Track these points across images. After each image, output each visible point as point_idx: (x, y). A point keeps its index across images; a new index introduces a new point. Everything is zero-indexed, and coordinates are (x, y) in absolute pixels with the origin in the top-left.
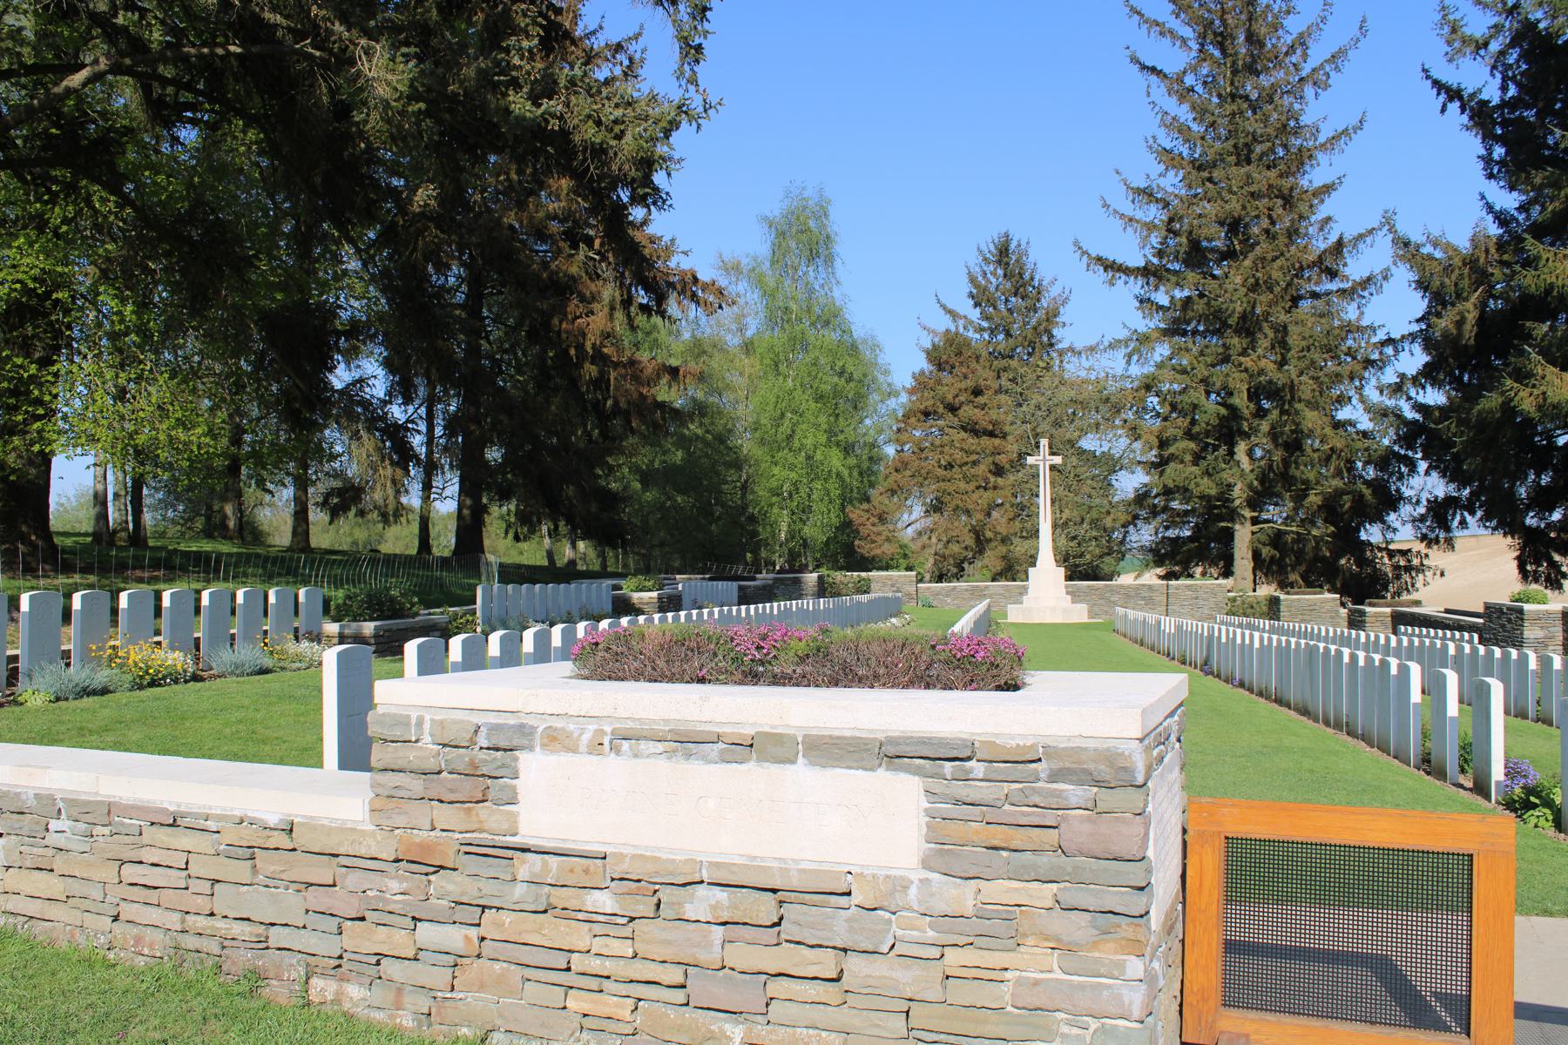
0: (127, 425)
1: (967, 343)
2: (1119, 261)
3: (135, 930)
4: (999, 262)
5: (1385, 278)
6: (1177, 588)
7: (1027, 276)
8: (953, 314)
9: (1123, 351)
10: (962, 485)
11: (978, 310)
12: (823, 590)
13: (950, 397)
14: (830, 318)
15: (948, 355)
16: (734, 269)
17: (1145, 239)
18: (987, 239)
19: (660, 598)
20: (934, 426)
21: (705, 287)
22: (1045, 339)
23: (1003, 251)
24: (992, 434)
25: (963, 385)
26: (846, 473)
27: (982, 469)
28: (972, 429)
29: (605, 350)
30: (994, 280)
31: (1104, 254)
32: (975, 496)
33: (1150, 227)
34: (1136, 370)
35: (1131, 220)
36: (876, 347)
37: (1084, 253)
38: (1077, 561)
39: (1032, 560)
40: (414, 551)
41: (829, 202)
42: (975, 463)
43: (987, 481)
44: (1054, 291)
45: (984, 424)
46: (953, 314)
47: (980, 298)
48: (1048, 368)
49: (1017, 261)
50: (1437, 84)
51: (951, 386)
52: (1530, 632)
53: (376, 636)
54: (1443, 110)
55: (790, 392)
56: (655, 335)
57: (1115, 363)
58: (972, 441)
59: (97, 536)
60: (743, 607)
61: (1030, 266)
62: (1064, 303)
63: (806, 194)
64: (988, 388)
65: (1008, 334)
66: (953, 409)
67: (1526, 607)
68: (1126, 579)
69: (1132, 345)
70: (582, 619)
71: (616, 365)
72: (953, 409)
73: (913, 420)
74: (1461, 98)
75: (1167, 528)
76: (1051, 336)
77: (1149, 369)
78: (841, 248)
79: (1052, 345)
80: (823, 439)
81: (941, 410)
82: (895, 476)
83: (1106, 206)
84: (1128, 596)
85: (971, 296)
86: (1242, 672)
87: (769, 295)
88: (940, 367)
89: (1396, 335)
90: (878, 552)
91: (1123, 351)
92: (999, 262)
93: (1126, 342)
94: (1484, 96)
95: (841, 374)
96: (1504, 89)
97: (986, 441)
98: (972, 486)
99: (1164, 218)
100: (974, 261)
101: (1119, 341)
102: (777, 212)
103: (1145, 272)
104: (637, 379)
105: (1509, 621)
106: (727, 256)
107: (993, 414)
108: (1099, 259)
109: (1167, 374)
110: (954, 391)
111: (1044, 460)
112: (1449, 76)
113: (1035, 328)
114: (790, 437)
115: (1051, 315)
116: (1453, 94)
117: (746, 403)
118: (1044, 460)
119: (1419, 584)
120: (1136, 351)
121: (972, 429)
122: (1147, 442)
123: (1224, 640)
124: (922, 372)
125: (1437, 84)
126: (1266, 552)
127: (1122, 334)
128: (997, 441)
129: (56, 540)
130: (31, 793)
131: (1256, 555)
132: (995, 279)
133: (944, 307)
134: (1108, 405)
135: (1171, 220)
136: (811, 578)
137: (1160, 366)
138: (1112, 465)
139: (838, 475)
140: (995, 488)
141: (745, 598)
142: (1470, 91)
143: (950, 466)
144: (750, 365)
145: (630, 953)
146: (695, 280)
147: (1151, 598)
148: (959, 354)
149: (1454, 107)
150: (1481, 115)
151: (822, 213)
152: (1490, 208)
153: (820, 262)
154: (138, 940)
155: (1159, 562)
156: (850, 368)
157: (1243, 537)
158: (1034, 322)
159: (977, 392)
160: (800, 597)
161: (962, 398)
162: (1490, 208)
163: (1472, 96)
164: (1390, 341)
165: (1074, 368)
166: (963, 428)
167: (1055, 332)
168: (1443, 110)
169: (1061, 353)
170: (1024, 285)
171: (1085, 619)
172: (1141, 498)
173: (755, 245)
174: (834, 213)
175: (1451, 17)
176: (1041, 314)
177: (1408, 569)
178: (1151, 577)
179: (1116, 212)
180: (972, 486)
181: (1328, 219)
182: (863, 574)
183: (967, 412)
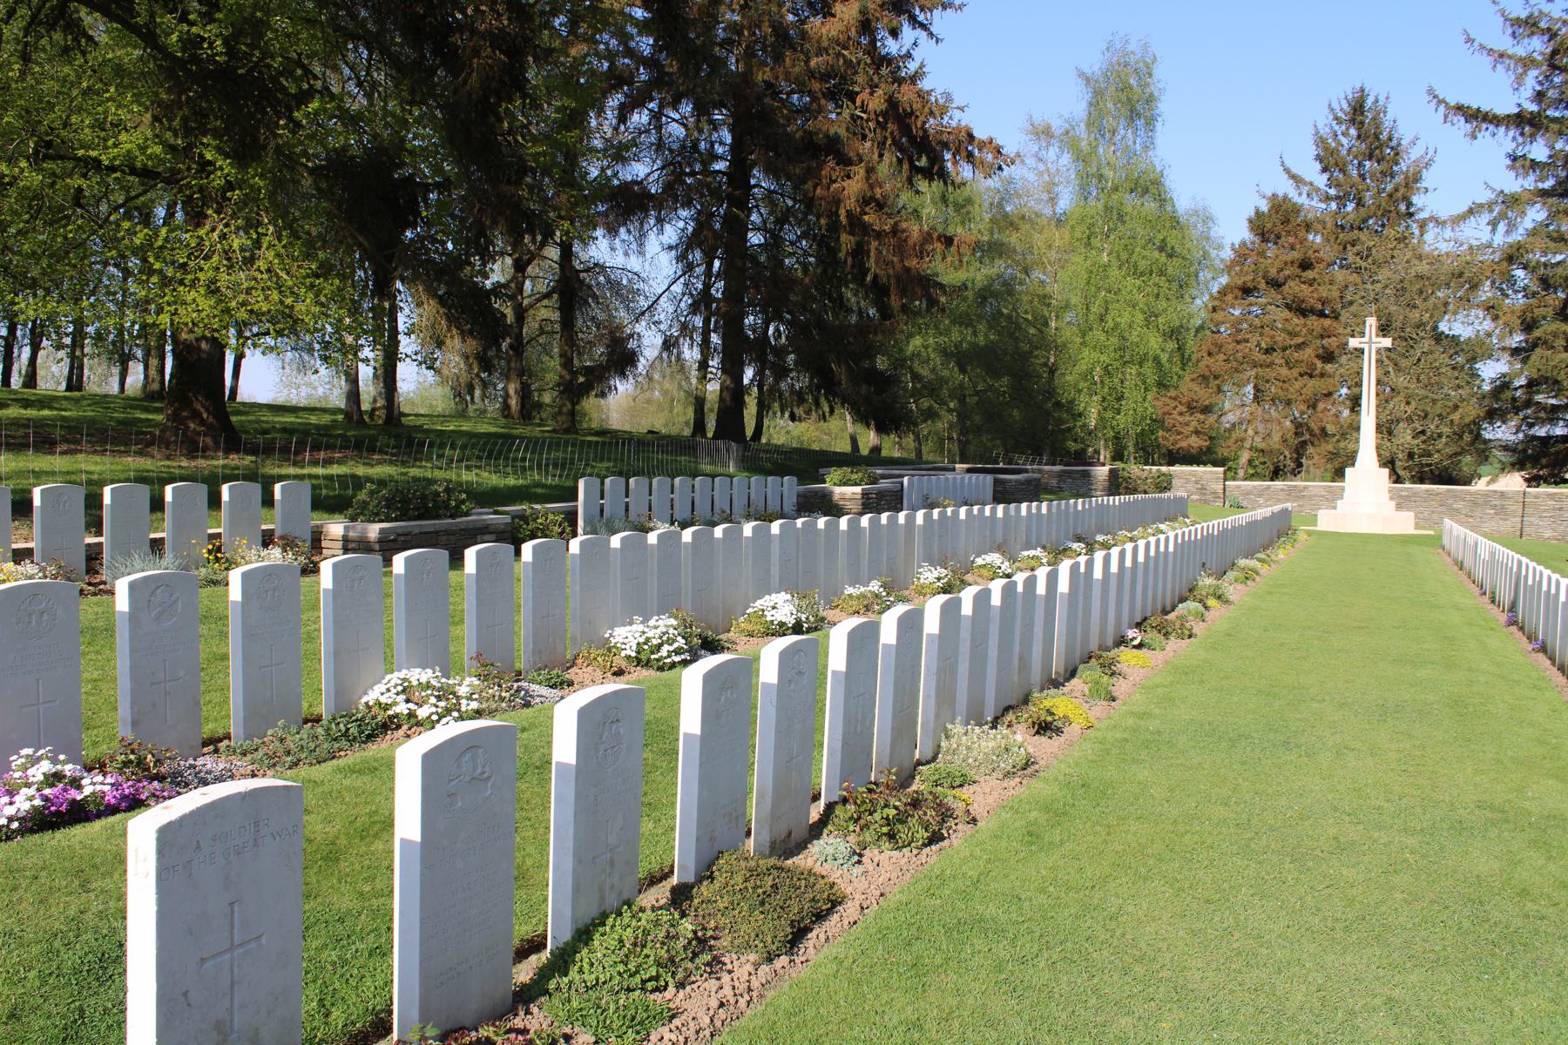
0: (132, 286)
1: (1296, 209)
2: (1485, 108)
4: (1353, 121)
6: (1536, 497)
7: (1384, 136)
8: (1295, 178)
9: (1486, 217)
10: (1284, 371)
11: (1326, 176)
12: (1116, 485)
14: (1150, 186)
15: (1276, 223)
16: (1043, 133)
17: (1520, 80)
18: (1339, 95)
19: (865, 494)
20: (1256, 305)
21: (982, 145)
22: (1403, 207)
23: (1357, 111)
24: (1321, 314)
25: (1289, 258)
26: (1164, 358)
27: (1308, 354)
28: (1300, 309)
29: (866, 218)
30: (1344, 141)
31: (1465, 102)
32: (1298, 385)
33: (1527, 63)
34: (1499, 239)
35: (1501, 56)
36: (1208, 219)
37: (1440, 102)
38: (1425, 460)
39: (1351, 459)
40: (687, 432)
41: (1155, 60)
42: (1299, 347)
43: (1313, 366)
44: (1415, 153)
45: (1312, 302)
46: (1295, 178)
47: (1329, 160)
48: (1402, 239)
49: (1374, 119)
51: (1275, 257)
53: (380, 541)
55: (1105, 267)
56: (969, 208)
57: (1477, 232)
58: (1297, 320)
59: (347, 414)
60: (1000, 508)
61: (1387, 124)
63: (1130, 48)
64: (1320, 261)
65: (1360, 204)
66: (1276, 284)
68: (1481, 485)
69: (1497, 209)
70: (748, 517)
71: (879, 235)
72: (1276, 284)
73: (1229, 297)
75: (1531, 426)
76: (1409, 204)
77: (1518, 236)
78: (1164, 107)
79: (1411, 215)
80: (1139, 318)
81: (1263, 285)
82: (1207, 361)
83: (1470, 40)
84: (1475, 504)
85: (1319, 158)
86: (1545, 634)
87: (1082, 158)
88: (1265, 240)
90: (1184, 444)
91: (1486, 217)
92: (1353, 121)
93: (1490, 206)
95: (1161, 249)
97: (1314, 322)
98: (1295, 372)
99: (1549, 51)
100: (1325, 122)
101: (1481, 206)
102: (1096, 68)
103: (1526, 123)
104: (901, 248)
106: (1037, 120)
107: (1324, 292)
108: (1459, 108)
109: (1540, 243)
110: (1278, 264)
111: (1370, 342)
113: (1390, 196)
114: (1102, 319)
115: (1412, 181)
117: (1060, 279)
118: (1370, 342)
120: (1502, 216)
121: (1300, 309)
122: (1506, 324)
123: (1530, 582)
124: (1243, 244)
127: (1484, 197)
128: (1327, 322)
129: (234, 419)
132: (1347, 140)
133: (1287, 171)
134: (1463, 279)
135: (1555, 52)
136: (1101, 472)
137: (1533, 233)
138: (1476, 351)
139: (1156, 360)
140: (1322, 375)
141: (1003, 495)
143: (1269, 351)
144: (1060, 237)
146: (971, 137)
148: (1286, 221)
151: (1145, 72)
153: (1140, 123)
155: (1519, 465)
156: (1171, 242)
158: (1389, 187)
159: (1305, 265)
160: (1087, 494)
161: (1287, 272)
165: (1437, 242)
166: (1288, 307)
167: (1415, 199)
169: (1423, 225)
170: (1380, 147)
171: (1410, 529)
172: (1503, 385)
173: (1067, 104)
174: (1158, 72)
176: (1399, 179)
178: (1513, 482)
179: (1482, 47)
180: (1295, 372)
182: (1164, 469)
183: (1294, 288)
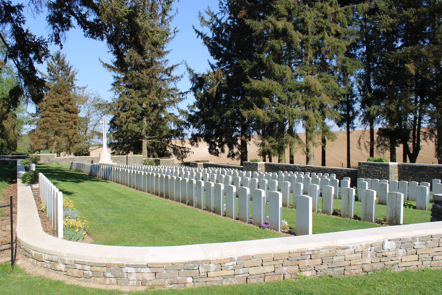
3: (437, 261)
5: (182, 77)
13: (61, 101)
24: (73, 112)
25: (66, 98)
28: (67, 110)
37: (101, 62)
42: (69, 121)
45: (72, 110)
49: (63, 60)
50: (196, 31)
52: (259, 169)
54: (198, 37)
58: (68, 114)
62: (76, 74)
67: (258, 163)
74: (202, 35)
76: (73, 83)
81: (59, 105)
89: (183, 92)
94: (208, 35)
96: (213, 35)
105: (253, 166)
108: (106, 64)
112: (200, 30)
115: (72, 77)
116: (200, 34)
119: (188, 156)
125: (196, 31)
126: (151, 147)
130: (410, 237)
131: (148, 149)
142: (204, 34)
145: (379, 261)
147: (122, 160)
149: (200, 37)
150: (206, 39)
152: (210, 63)
154: (438, 263)
157: (145, 143)
161: (65, 102)
162: (210, 63)
163: (204, 35)
164: (181, 93)
167: (74, 82)
168: (198, 37)
175: (202, 16)
177: (185, 152)
181: (167, 60)
